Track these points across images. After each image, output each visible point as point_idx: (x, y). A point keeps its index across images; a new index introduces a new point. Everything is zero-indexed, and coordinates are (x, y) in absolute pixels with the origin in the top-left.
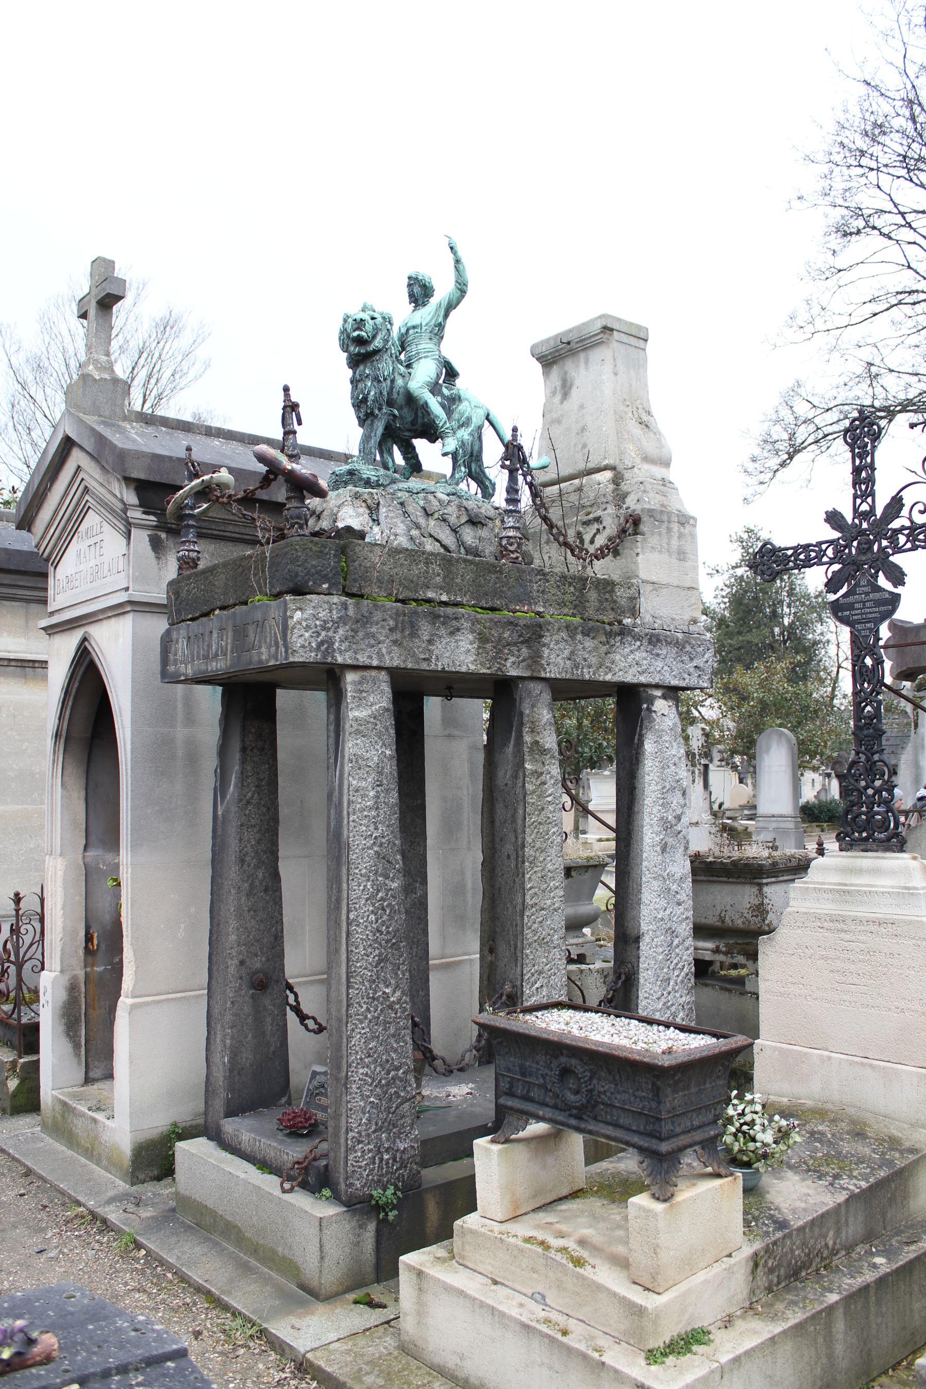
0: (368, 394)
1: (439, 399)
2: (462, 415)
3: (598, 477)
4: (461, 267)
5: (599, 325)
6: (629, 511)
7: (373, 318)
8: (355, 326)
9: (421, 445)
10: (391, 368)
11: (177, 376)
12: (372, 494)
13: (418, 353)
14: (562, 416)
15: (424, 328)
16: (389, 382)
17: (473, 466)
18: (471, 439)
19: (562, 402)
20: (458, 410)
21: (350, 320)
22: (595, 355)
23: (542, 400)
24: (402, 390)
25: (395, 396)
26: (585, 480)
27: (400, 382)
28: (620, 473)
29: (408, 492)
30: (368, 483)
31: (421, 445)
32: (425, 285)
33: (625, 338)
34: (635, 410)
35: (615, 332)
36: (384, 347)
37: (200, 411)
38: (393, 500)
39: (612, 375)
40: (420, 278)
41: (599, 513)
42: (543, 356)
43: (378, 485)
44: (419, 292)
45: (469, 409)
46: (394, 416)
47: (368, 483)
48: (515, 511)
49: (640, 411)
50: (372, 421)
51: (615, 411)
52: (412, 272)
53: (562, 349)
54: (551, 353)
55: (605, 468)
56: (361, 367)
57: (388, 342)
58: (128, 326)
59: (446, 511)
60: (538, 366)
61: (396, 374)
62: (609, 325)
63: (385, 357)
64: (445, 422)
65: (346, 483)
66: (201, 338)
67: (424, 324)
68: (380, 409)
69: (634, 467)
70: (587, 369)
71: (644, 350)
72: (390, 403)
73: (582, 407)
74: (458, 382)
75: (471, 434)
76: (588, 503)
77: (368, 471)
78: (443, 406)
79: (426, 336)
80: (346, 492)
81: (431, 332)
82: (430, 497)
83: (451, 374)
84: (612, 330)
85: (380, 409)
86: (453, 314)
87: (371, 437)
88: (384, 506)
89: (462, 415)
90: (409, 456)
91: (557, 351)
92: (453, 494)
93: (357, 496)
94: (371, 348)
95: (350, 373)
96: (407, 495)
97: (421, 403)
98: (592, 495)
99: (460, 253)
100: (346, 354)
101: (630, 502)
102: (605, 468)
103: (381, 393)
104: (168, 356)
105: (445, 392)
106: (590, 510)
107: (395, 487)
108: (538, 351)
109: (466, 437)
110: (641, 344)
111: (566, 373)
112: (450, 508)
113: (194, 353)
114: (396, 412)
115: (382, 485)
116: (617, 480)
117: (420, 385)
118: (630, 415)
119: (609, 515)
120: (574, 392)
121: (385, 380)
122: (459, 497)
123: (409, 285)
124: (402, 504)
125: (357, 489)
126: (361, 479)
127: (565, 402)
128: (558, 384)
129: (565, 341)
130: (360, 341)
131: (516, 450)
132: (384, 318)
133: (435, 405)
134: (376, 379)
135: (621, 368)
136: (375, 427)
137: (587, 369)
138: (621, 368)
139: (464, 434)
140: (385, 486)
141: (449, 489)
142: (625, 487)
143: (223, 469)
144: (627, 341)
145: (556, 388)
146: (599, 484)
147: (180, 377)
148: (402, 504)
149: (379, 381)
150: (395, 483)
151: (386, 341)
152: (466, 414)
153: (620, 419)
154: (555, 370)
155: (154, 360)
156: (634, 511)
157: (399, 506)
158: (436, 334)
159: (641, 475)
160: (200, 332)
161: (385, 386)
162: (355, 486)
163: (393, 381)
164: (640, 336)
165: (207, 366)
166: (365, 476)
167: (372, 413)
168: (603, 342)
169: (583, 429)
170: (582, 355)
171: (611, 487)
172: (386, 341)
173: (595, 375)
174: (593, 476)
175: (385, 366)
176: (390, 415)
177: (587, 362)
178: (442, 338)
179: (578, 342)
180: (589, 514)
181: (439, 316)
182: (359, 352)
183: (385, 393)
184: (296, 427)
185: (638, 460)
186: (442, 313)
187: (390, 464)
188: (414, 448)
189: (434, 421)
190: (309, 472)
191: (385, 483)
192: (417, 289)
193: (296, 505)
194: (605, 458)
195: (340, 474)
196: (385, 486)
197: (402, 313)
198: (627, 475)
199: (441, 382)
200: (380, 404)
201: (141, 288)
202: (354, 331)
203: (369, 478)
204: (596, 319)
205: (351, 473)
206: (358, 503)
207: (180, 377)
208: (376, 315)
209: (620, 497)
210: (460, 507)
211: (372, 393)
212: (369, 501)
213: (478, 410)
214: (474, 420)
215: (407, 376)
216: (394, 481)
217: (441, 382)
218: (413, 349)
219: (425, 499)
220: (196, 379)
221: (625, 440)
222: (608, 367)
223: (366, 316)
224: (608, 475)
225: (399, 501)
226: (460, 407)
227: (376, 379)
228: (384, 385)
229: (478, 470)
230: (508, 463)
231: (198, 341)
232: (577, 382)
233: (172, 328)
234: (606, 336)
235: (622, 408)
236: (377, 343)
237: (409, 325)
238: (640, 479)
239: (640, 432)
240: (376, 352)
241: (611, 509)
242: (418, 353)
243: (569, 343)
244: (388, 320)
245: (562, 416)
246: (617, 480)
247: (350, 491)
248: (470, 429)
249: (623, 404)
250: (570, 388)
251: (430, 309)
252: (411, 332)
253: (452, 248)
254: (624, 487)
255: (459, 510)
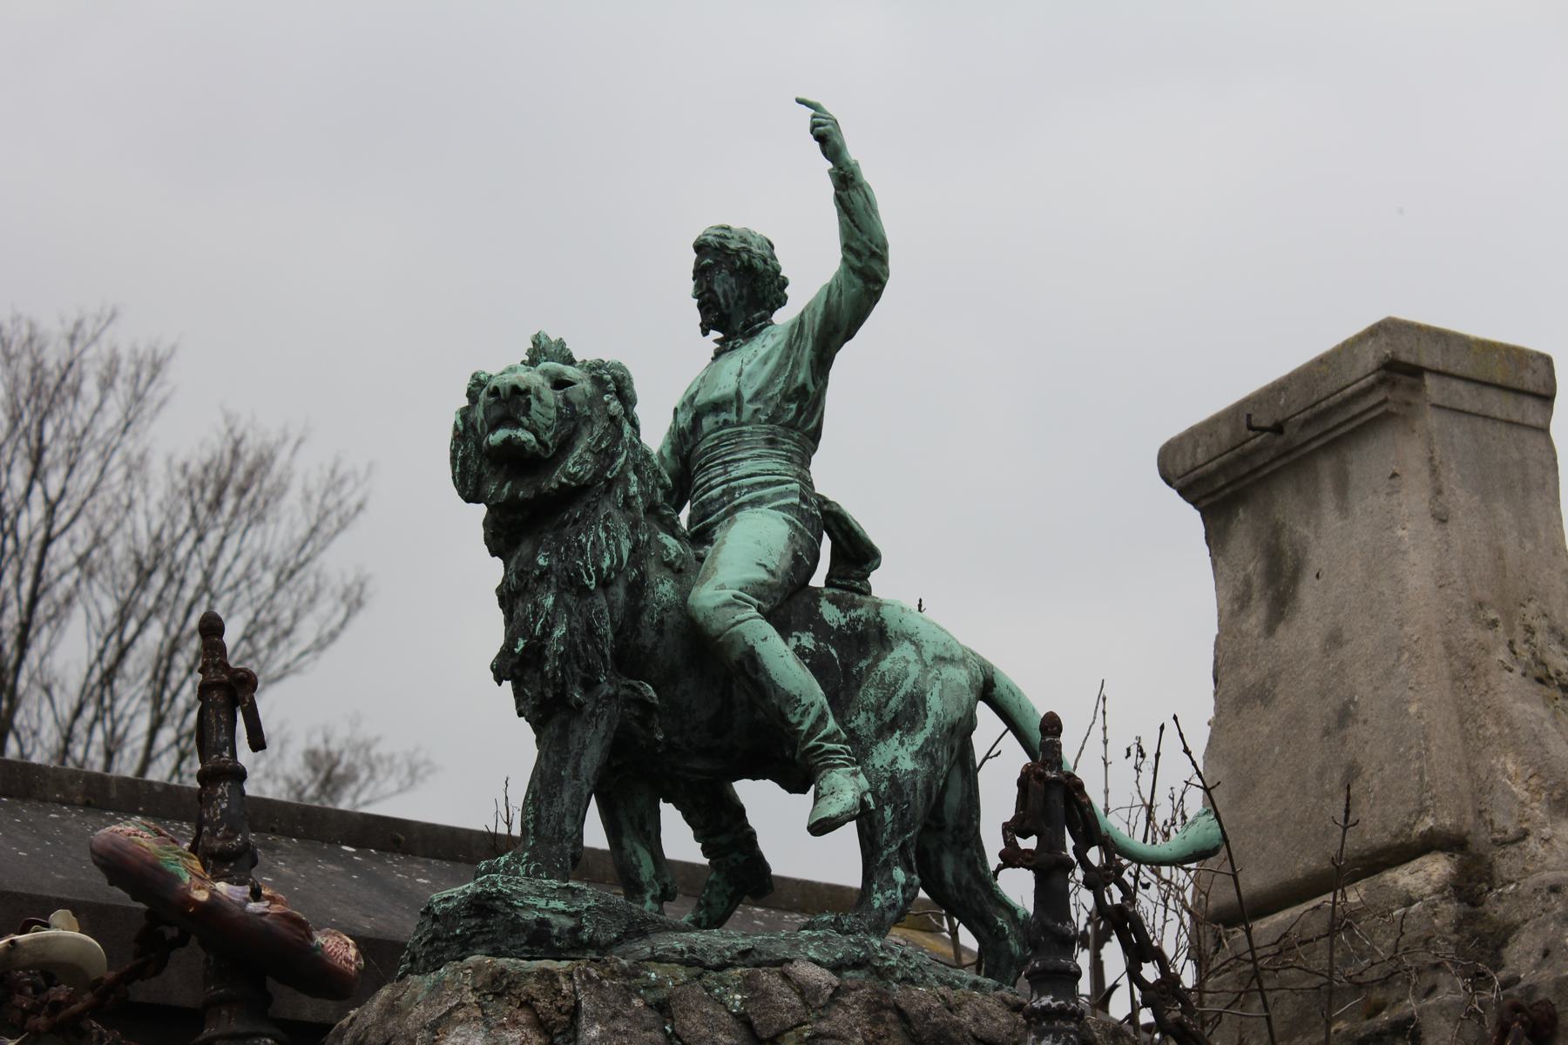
0: (546, 633)
1: (808, 640)
2: (891, 688)
3: (1405, 878)
4: (859, 200)
5: (1369, 359)
6: (1515, 991)
7: (560, 383)
8: (497, 412)
9: (763, 803)
10: (626, 546)
11: (262, 642)
12: (551, 976)
13: (730, 492)
14: (1274, 676)
15: (748, 409)
16: (620, 591)
17: (949, 864)
18: (924, 769)
19: (1270, 629)
20: (875, 676)
21: (483, 395)
22: (1369, 462)
23: (1209, 628)
24: (671, 619)
25: (648, 638)
26: (1354, 895)
27: (665, 589)
28: (1479, 858)
29: (688, 964)
30: (540, 940)
31: (763, 803)
32: (749, 269)
33: (1465, 396)
34: (1519, 635)
35: (1429, 380)
36: (598, 475)
37: (334, 747)
38: (627, 993)
39: (1430, 525)
40: (733, 245)
41: (1411, 1005)
42: (1199, 481)
43: (574, 945)
44: (734, 285)
45: (914, 670)
46: (644, 704)
47: (540, 940)
48: (1061, 1013)
49: (1540, 638)
50: (564, 726)
51: (1448, 646)
52: (701, 225)
53: (1258, 450)
54: (1222, 469)
55: (1430, 844)
56: (525, 549)
57: (614, 457)
58: (105, 497)
59: (824, 1026)
60: (1191, 520)
61: (652, 567)
62: (1404, 357)
63: (606, 508)
64: (822, 718)
65: (465, 946)
66: (333, 519)
67: (747, 394)
68: (589, 685)
69: (1525, 834)
70: (1344, 509)
71: (1544, 431)
72: (629, 660)
73: (1335, 640)
74: (880, 582)
75: (921, 754)
76: (1375, 973)
77: (543, 900)
78: (818, 664)
79: (756, 433)
80: (461, 976)
81: (772, 419)
82: (769, 979)
83: (856, 556)
84: (1416, 372)
85: (589, 685)
86: (846, 358)
87: (560, 781)
88: (595, 1018)
89: (891, 688)
90: (723, 839)
91: (1243, 458)
92: (857, 965)
93: (498, 987)
94: (557, 479)
95: (495, 570)
96: (682, 974)
97: (735, 655)
98: (1384, 944)
99: (855, 151)
100: (481, 510)
101: (1521, 958)
102: (1430, 844)
103: (590, 631)
104: (230, 581)
105: (830, 613)
106: (1378, 995)
107: (643, 948)
108: (1182, 464)
109: (907, 764)
110: (1529, 411)
111: (1277, 530)
112: (840, 1015)
113: (314, 566)
114: (650, 692)
115: (592, 944)
116: (1472, 882)
117: (727, 595)
118: (1502, 654)
119: (1442, 1009)
120: (1308, 592)
121: (605, 584)
122: (883, 974)
123: (700, 273)
124: (662, 1008)
125: (502, 962)
126: (516, 927)
127: (1281, 630)
128: (1254, 567)
129: (1266, 422)
130: (512, 460)
131: (1057, 796)
132: (598, 381)
133: (782, 659)
134: (572, 585)
135: (1461, 498)
136: (574, 747)
137: (1344, 509)
138: (1461, 498)
139: (899, 755)
140: (603, 948)
141: (842, 947)
142: (1501, 909)
143: (59, 916)
144: (1476, 406)
145: (1247, 583)
146: (1410, 902)
147: (274, 643)
148: (662, 1008)
149: (584, 591)
150: (643, 934)
151: (606, 456)
152: (907, 686)
153: (1467, 670)
154: (1244, 525)
155: (188, 594)
156: (1531, 990)
157: (650, 1016)
158: (791, 426)
159: (1552, 860)
160: (331, 501)
161: (606, 610)
162: (497, 953)
163: (638, 588)
164: (1522, 383)
165: (354, 602)
166: (529, 916)
167: (561, 699)
168: (1388, 415)
169: (1345, 716)
170: (1326, 467)
171: (1450, 910)
172: (606, 456)
173: (1386, 535)
174: (1388, 875)
175: (607, 541)
176: (628, 702)
177: (1342, 487)
178: (815, 435)
179: (1307, 423)
180: (1377, 1009)
181: (796, 365)
182: (513, 496)
183: (606, 629)
184: (244, 755)
185: (1539, 811)
186: (807, 353)
187: (647, 870)
188: (741, 811)
189: (782, 716)
190: (276, 909)
191: (602, 937)
192: (723, 284)
193: (236, 1027)
194: (1422, 811)
195: (446, 914)
196: (603, 948)
197: (668, 364)
198: (1506, 864)
199: (818, 580)
200: (589, 669)
201: (145, 376)
202: (494, 428)
203: (543, 923)
204: (1361, 339)
205: (480, 906)
206: (503, 1010)
207: (274, 643)
208: (570, 372)
209: (1482, 942)
210: (877, 1008)
211: (558, 632)
212: (543, 1003)
213: (949, 672)
214: (934, 702)
215: (685, 572)
216: (639, 929)
217: (818, 580)
218: (714, 483)
219: (748, 985)
220: (320, 645)
221: (1488, 741)
222: (1414, 498)
223: (533, 378)
224: (1437, 867)
225: (651, 997)
226: (885, 665)
227: (572, 585)
228: (601, 601)
229: (966, 876)
230: (1030, 843)
231: (325, 529)
232: (1317, 558)
233: (242, 491)
234: (1399, 394)
235: (1472, 633)
236: (577, 463)
237: (701, 399)
238: (1549, 876)
239: (1541, 711)
240: (575, 493)
241: (1451, 990)
242: (730, 492)
243: (1278, 428)
244: (615, 385)
245: (1274, 676)
246: (1472, 882)
247: (477, 969)
248: (920, 739)
249: (1474, 619)
250: (1295, 578)
251: (770, 343)
252: (708, 422)
253: (822, 139)
254: (1497, 909)
255: (876, 1020)
